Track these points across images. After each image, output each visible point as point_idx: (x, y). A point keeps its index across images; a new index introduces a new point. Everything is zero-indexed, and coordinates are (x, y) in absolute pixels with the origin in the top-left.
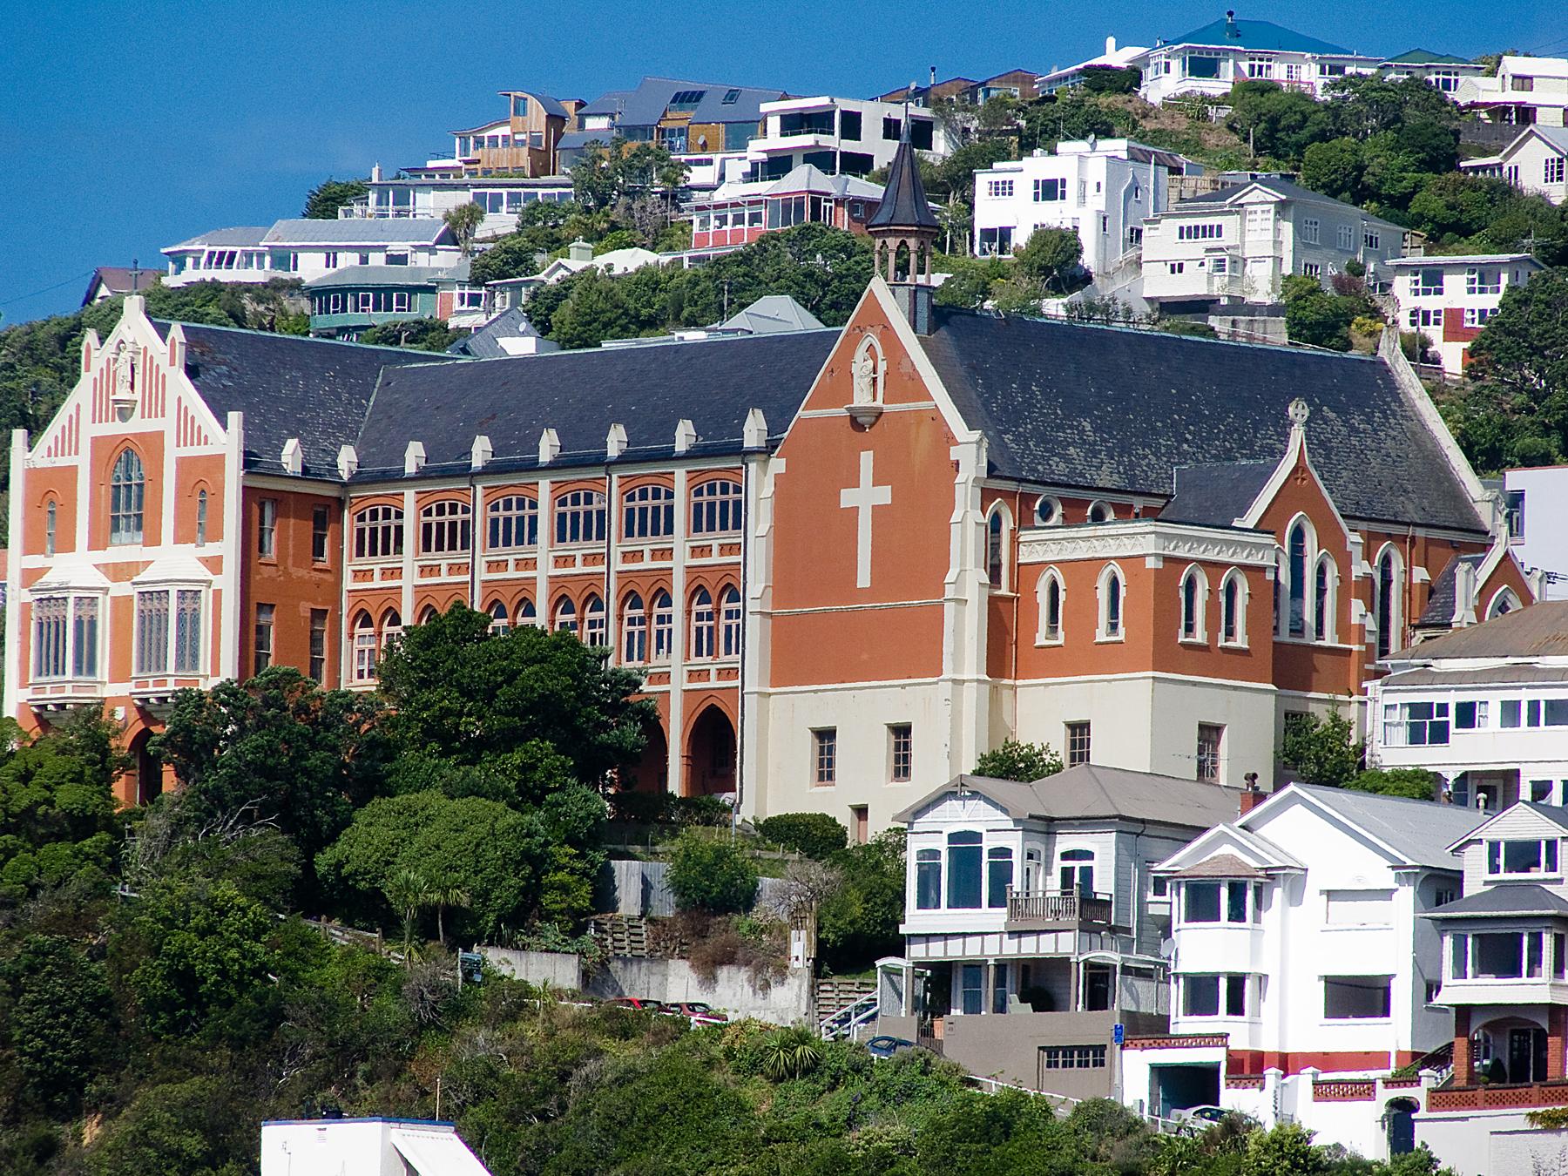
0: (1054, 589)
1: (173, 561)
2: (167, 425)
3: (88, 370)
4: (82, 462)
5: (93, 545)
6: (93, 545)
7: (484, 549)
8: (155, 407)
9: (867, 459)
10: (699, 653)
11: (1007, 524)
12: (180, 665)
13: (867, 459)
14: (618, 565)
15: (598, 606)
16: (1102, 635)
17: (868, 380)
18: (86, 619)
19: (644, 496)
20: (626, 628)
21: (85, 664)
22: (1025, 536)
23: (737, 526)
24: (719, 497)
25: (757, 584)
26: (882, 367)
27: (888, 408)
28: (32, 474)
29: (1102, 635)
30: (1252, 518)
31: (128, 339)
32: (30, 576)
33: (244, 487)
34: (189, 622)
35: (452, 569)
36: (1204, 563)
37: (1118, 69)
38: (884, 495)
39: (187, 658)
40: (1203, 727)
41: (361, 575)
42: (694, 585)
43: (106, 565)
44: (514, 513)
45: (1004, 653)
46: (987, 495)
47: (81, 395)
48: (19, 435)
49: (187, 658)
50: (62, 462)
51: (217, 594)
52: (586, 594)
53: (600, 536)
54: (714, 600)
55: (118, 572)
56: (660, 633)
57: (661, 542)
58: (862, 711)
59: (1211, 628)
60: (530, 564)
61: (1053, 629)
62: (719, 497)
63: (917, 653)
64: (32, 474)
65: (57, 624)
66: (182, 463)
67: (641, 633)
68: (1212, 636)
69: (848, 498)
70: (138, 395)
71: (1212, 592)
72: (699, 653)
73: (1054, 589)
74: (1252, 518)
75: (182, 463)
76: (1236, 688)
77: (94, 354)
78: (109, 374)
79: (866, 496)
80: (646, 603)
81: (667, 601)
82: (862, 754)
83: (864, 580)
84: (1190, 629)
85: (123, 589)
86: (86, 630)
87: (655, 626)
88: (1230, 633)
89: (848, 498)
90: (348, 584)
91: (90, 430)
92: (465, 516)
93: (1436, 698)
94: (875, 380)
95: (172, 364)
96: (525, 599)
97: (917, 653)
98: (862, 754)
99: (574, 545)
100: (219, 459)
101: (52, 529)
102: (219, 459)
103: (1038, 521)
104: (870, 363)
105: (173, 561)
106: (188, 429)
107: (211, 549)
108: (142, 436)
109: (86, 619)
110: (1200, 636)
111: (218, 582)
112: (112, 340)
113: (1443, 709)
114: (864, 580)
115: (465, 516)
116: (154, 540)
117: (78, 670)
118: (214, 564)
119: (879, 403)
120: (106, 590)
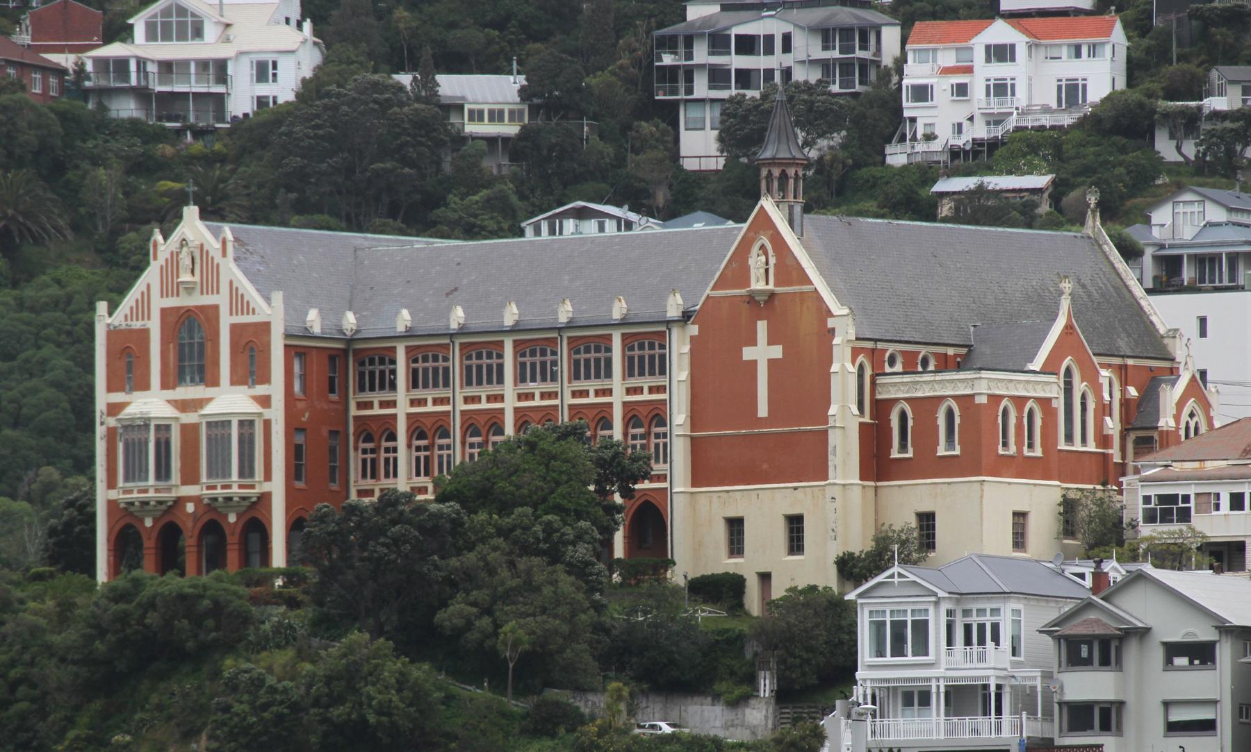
0: (903, 416)
1: (229, 400)
2: (221, 300)
3: (155, 258)
4: (154, 326)
5: (165, 386)
6: (165, 386)
7: (462, 387)
8: (210, 284)
9: (762, 327)
10: (418, 474)
11: (868, 373)
12: (241, 475)
13: (762, 327)
14: (461, 406)
15: (446, 434)
16: (941, 451)
17: (762, 271)
18: (163, 441)
19: (425, 359)
20: (468, 450)
21: (163, 472)
22: (881, 380)
23: (663, 372)
24: (647, 352)
25: (680, 417)
26: (772, 261)
27: (780, 290)
28: (112, 333)
29: (941, 451)
30: (1036, 365)
31: (190, 236)
32: (114, 409)
33: (286, 346)
34: (246, 443)
35: (436, 402)
36: (1012, 398)
37: (318, 69)
38: (777, 352)
39: (247, 469)
40: (1016, 514)
41: (361, 405)
42: (630, 415)
43: (176, 401)
44: (485, 361)
45: (877, 464)
46: (855, 352)
47: (151, 276)
48: (102, 307)
49: (247, 469)
50: (137, 325)
51: (267, 424)
52: (436, 426)
53: (446, 384)
54: (646, 425)
55: (183, 406)
56: (387, 460)
57: (494, 389)
58: (765, 506)
59: (1019, 444)
60: (500, 398)
61: (903, 447)
62: (647, 352)
63: (809, 461)
64: (112, 333)
65: (246, 443)
66: (235, 328)
67: (426, 458)
68: (1020, 450)
69: (748, 353)
70: (197, 278)
71: (1019, 419)
72: (418, 474)
73: (903, 416)
74: (1036, 365)
75: (235, 328)
76: (1035, 485)
77: (161, 248)
78: (174, 261)
79: (762, 352)
80: (484, 431)
81: (392, 437)
82: (764, 537)
83: (763, 411)
84: (1005, 444)
85: (190, 418)
86: (163, 448)
87: (383, 455)
88: (1031, 446)
89: (748, 353)
90: (353, 411)
91: (158, 303)
92: (445, 364)
93: (1181, 491)
94: (767, 270)
95: (224, 254)
96: (657, 415)
97: (809, 461)
98: (764, 537)
99: (426, 391)
100: (265, 327)
101: (130, 371)
102: (265, 327)
103: (888, 369)
104: (763, 258)
105: (229, 400)
106: (239, 303)
107: (261, 390)
108: (202, 309)
109: (163, 441)
110: (1012, 450)
111: (267, 413)
112: (175, 237)
113: (1186, 498)
114: (763, 411)
115: (445, 364)
116: (215, 382)
117: (158, 477)
118: (265, 401)
119: (771, 286)
120: (177, 419)
